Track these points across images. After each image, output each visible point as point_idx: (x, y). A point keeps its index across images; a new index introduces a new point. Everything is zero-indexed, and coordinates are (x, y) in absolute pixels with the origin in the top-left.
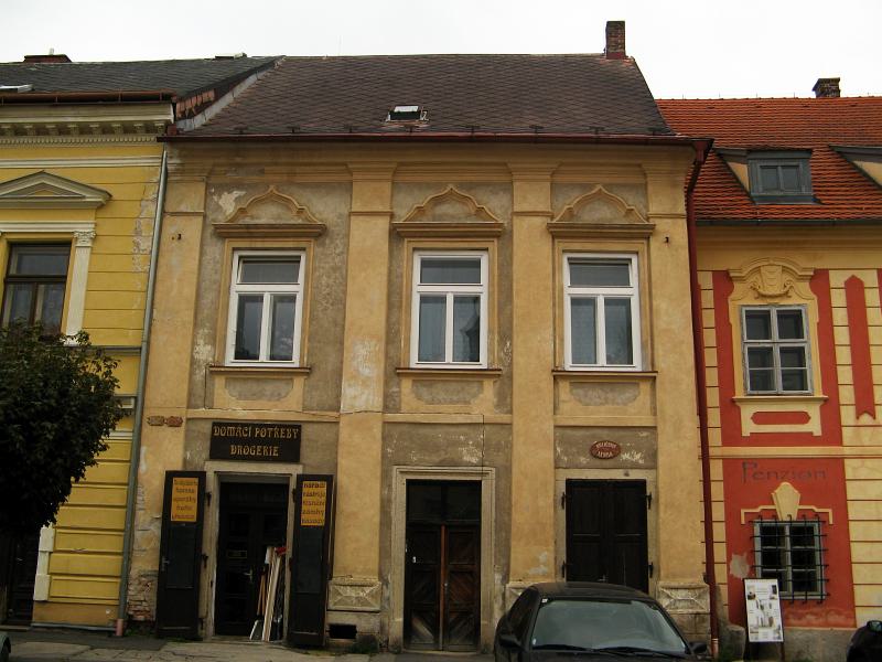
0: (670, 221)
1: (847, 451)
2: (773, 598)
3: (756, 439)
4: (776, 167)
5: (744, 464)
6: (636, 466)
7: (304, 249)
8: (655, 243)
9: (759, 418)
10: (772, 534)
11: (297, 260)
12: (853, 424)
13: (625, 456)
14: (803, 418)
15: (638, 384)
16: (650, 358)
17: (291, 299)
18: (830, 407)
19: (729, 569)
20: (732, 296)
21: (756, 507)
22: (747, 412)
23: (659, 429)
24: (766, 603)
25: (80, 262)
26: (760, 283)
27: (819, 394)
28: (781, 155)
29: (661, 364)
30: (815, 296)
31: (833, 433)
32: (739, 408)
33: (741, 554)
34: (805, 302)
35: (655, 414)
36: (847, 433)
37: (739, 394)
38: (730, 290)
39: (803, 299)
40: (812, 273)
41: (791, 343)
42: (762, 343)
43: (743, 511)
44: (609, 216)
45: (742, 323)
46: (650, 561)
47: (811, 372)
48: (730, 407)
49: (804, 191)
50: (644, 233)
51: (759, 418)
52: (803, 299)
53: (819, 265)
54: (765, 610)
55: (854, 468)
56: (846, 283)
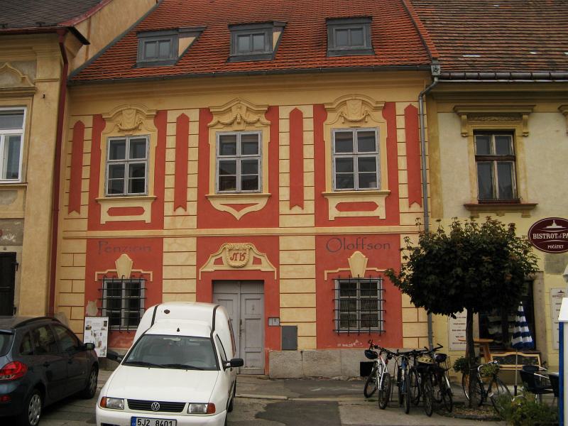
0: (47, 83)
1: (165, 233)
2: (103, 329)
3: (110, 226)
4: (346, 30)
5: (100, 242)
6: (11, 244)
7: (25, 106)
8: (37, 99)
9: (112, 212)
10: (114, 288)
11: (21, 113)
12: (172, 215)
13: (5, 237)
14: (373, 206)
15: (17, 191)
16: (25, 176)
17: (18, 138)
18: (158, 203)
19: (85, 311)
20: (104, 131)
21: (105, 270)
22: (105, 208)
23: (26, 219)
24: (98, 332)
25: (25, 112)
26: (346, 112)
27: (151, 195)
28: (158, 34)
29: (30, 178)
30: (385, 121)
31: (158, 221)
32: (327, 200)
33: (93, 300)
34: (149, 133)
35: (24, 210)
36: (167, 220)
37: (101, 196)
38: (103, 127)
39: (149, 131)
40: (266, 109)
41: (137, 161)
42: (119, 162)
43: (326, 272)
44: (12, 83)
45: (107, 149)
46: (15, 304)
47: (261, 178)
48: (95, 205)
49: (365, 47)
50: (29, 93)
51: (112, 212)
52: (149, 131)
53: (161, 107)
54: (97, 337)
55: (170, 245)
56: (178, 119)
